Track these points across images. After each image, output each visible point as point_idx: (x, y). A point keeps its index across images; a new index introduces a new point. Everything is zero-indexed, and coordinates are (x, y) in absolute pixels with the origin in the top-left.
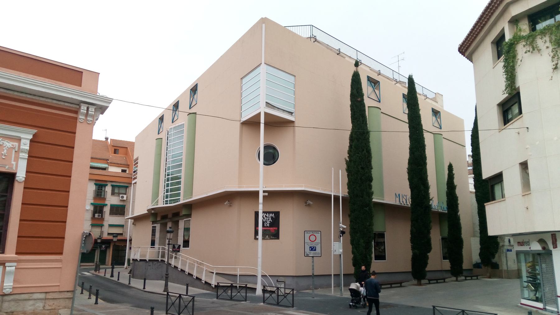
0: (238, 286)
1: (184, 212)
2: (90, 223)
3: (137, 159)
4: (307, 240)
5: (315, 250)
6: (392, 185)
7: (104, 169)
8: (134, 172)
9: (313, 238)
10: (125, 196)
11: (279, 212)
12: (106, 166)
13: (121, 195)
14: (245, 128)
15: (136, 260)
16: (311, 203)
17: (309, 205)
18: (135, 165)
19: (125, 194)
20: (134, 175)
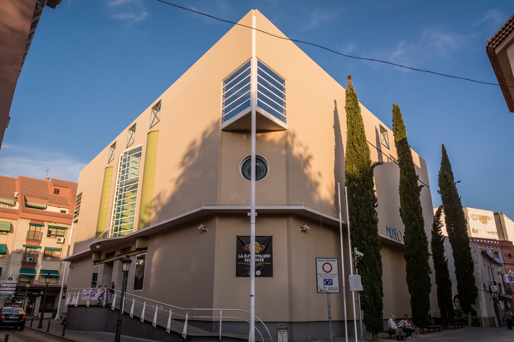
0: (220, 334)
1: (138, 244)
2: (19, 267)
3: (81, 194)
4: (320, 271)
5: (331, 284)
6: (389, 222)
7: (43, 209)
8: (76, 213)
9: (327, 268)
10: (62, 239)
11: (271, 238)
12: (45, 206)
13: (58, 238)
14: (225, 133)
15: (73, 306)
16: (308, 228)
17: (304, 231)
18: (78, 201)
19: (63, 236)
20: (75, 217)
